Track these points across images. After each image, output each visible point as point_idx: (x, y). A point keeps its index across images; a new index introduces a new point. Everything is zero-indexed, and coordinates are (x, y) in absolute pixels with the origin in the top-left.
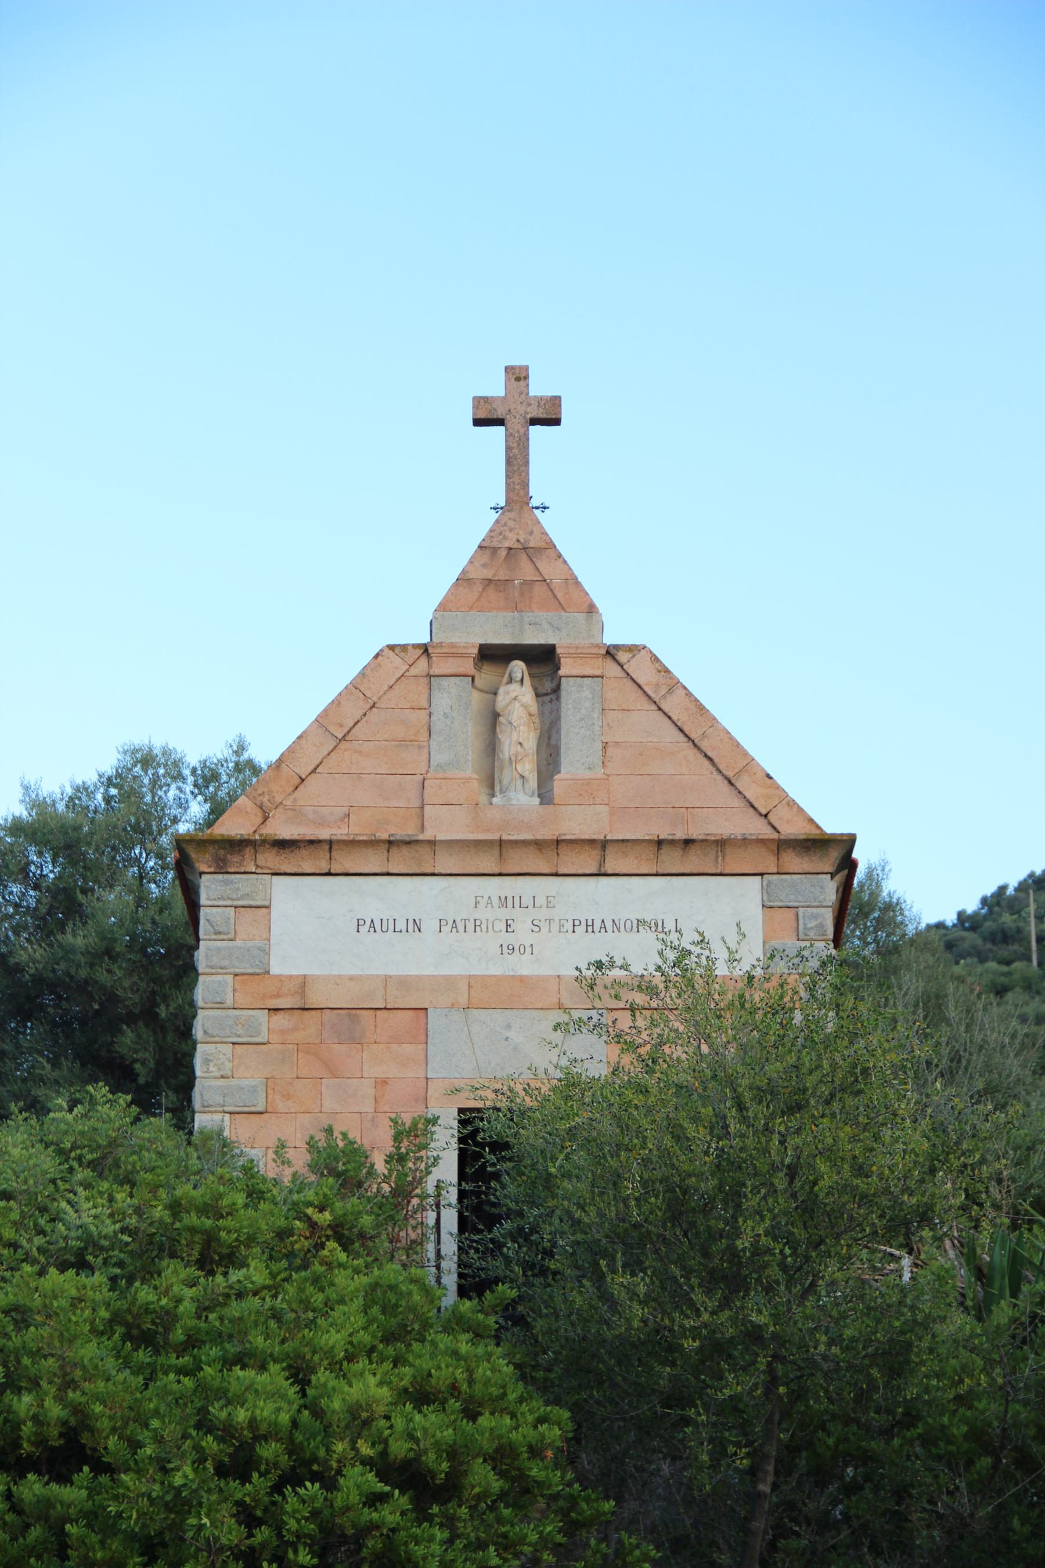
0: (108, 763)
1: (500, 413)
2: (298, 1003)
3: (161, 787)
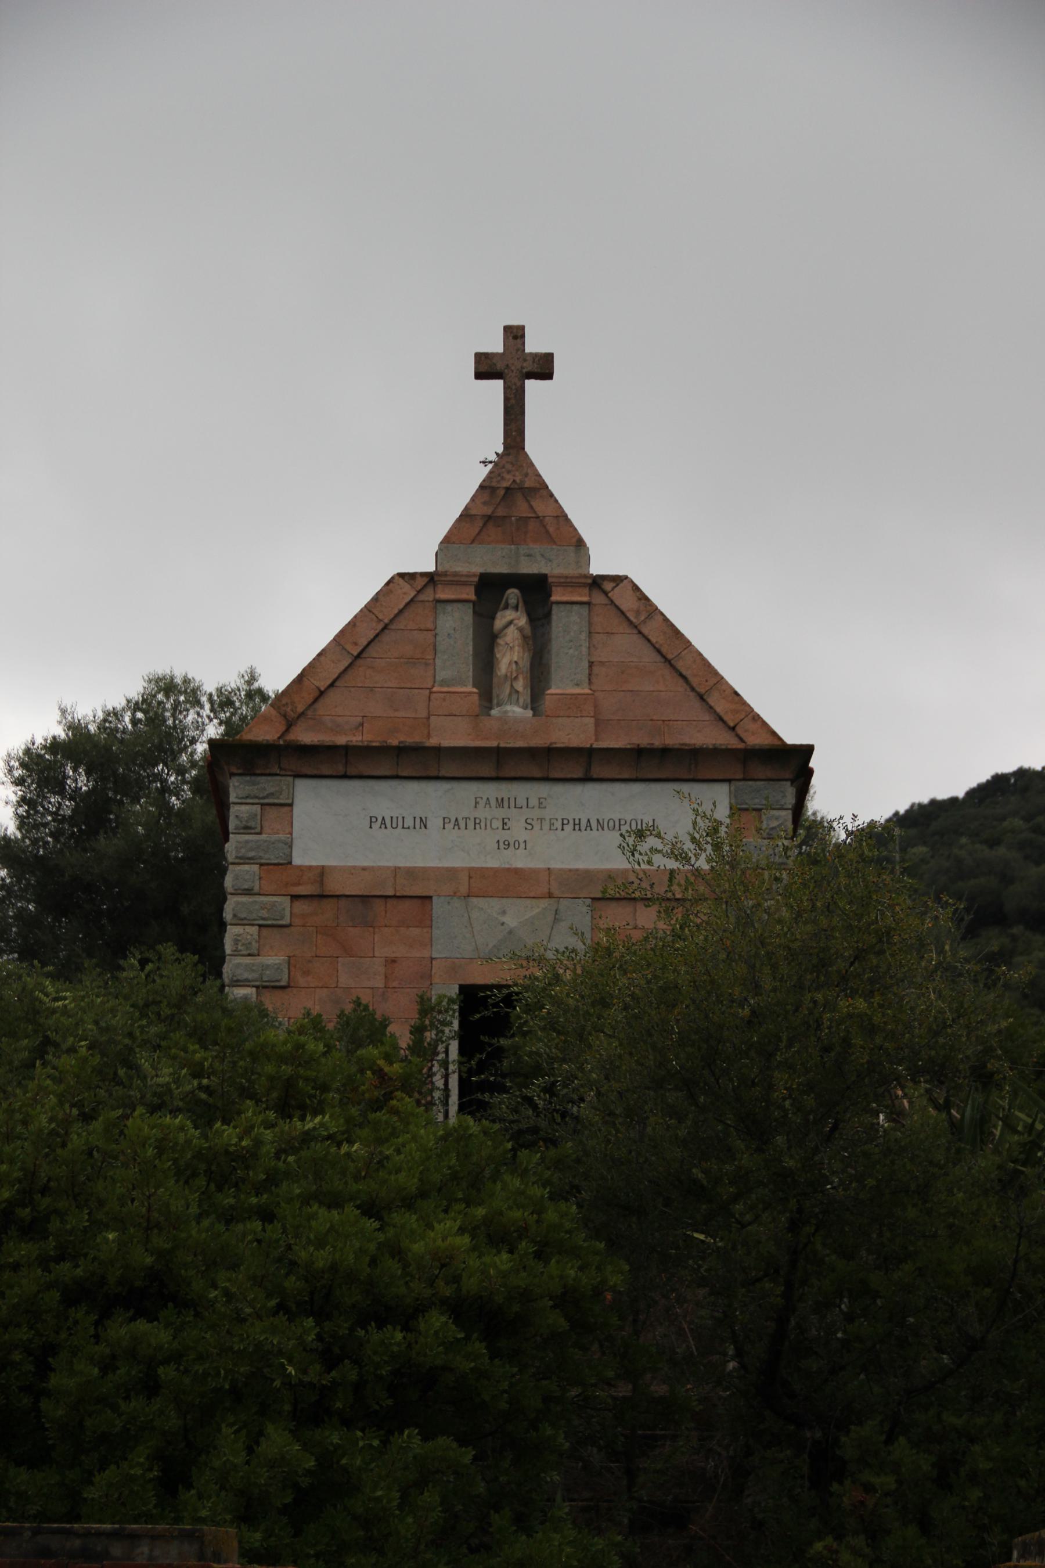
0: (135, 689)
1: (500, 366)
2: (318, 891)
3: (181, 712)
